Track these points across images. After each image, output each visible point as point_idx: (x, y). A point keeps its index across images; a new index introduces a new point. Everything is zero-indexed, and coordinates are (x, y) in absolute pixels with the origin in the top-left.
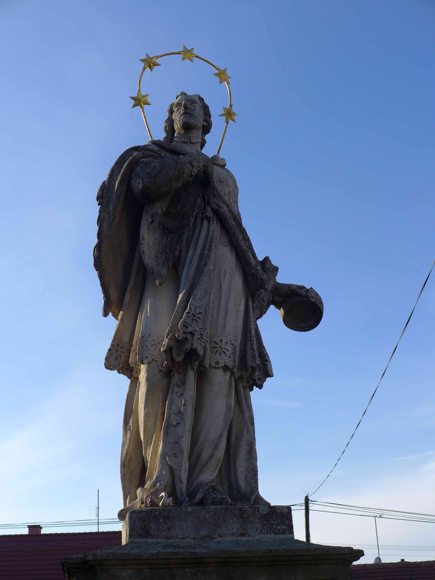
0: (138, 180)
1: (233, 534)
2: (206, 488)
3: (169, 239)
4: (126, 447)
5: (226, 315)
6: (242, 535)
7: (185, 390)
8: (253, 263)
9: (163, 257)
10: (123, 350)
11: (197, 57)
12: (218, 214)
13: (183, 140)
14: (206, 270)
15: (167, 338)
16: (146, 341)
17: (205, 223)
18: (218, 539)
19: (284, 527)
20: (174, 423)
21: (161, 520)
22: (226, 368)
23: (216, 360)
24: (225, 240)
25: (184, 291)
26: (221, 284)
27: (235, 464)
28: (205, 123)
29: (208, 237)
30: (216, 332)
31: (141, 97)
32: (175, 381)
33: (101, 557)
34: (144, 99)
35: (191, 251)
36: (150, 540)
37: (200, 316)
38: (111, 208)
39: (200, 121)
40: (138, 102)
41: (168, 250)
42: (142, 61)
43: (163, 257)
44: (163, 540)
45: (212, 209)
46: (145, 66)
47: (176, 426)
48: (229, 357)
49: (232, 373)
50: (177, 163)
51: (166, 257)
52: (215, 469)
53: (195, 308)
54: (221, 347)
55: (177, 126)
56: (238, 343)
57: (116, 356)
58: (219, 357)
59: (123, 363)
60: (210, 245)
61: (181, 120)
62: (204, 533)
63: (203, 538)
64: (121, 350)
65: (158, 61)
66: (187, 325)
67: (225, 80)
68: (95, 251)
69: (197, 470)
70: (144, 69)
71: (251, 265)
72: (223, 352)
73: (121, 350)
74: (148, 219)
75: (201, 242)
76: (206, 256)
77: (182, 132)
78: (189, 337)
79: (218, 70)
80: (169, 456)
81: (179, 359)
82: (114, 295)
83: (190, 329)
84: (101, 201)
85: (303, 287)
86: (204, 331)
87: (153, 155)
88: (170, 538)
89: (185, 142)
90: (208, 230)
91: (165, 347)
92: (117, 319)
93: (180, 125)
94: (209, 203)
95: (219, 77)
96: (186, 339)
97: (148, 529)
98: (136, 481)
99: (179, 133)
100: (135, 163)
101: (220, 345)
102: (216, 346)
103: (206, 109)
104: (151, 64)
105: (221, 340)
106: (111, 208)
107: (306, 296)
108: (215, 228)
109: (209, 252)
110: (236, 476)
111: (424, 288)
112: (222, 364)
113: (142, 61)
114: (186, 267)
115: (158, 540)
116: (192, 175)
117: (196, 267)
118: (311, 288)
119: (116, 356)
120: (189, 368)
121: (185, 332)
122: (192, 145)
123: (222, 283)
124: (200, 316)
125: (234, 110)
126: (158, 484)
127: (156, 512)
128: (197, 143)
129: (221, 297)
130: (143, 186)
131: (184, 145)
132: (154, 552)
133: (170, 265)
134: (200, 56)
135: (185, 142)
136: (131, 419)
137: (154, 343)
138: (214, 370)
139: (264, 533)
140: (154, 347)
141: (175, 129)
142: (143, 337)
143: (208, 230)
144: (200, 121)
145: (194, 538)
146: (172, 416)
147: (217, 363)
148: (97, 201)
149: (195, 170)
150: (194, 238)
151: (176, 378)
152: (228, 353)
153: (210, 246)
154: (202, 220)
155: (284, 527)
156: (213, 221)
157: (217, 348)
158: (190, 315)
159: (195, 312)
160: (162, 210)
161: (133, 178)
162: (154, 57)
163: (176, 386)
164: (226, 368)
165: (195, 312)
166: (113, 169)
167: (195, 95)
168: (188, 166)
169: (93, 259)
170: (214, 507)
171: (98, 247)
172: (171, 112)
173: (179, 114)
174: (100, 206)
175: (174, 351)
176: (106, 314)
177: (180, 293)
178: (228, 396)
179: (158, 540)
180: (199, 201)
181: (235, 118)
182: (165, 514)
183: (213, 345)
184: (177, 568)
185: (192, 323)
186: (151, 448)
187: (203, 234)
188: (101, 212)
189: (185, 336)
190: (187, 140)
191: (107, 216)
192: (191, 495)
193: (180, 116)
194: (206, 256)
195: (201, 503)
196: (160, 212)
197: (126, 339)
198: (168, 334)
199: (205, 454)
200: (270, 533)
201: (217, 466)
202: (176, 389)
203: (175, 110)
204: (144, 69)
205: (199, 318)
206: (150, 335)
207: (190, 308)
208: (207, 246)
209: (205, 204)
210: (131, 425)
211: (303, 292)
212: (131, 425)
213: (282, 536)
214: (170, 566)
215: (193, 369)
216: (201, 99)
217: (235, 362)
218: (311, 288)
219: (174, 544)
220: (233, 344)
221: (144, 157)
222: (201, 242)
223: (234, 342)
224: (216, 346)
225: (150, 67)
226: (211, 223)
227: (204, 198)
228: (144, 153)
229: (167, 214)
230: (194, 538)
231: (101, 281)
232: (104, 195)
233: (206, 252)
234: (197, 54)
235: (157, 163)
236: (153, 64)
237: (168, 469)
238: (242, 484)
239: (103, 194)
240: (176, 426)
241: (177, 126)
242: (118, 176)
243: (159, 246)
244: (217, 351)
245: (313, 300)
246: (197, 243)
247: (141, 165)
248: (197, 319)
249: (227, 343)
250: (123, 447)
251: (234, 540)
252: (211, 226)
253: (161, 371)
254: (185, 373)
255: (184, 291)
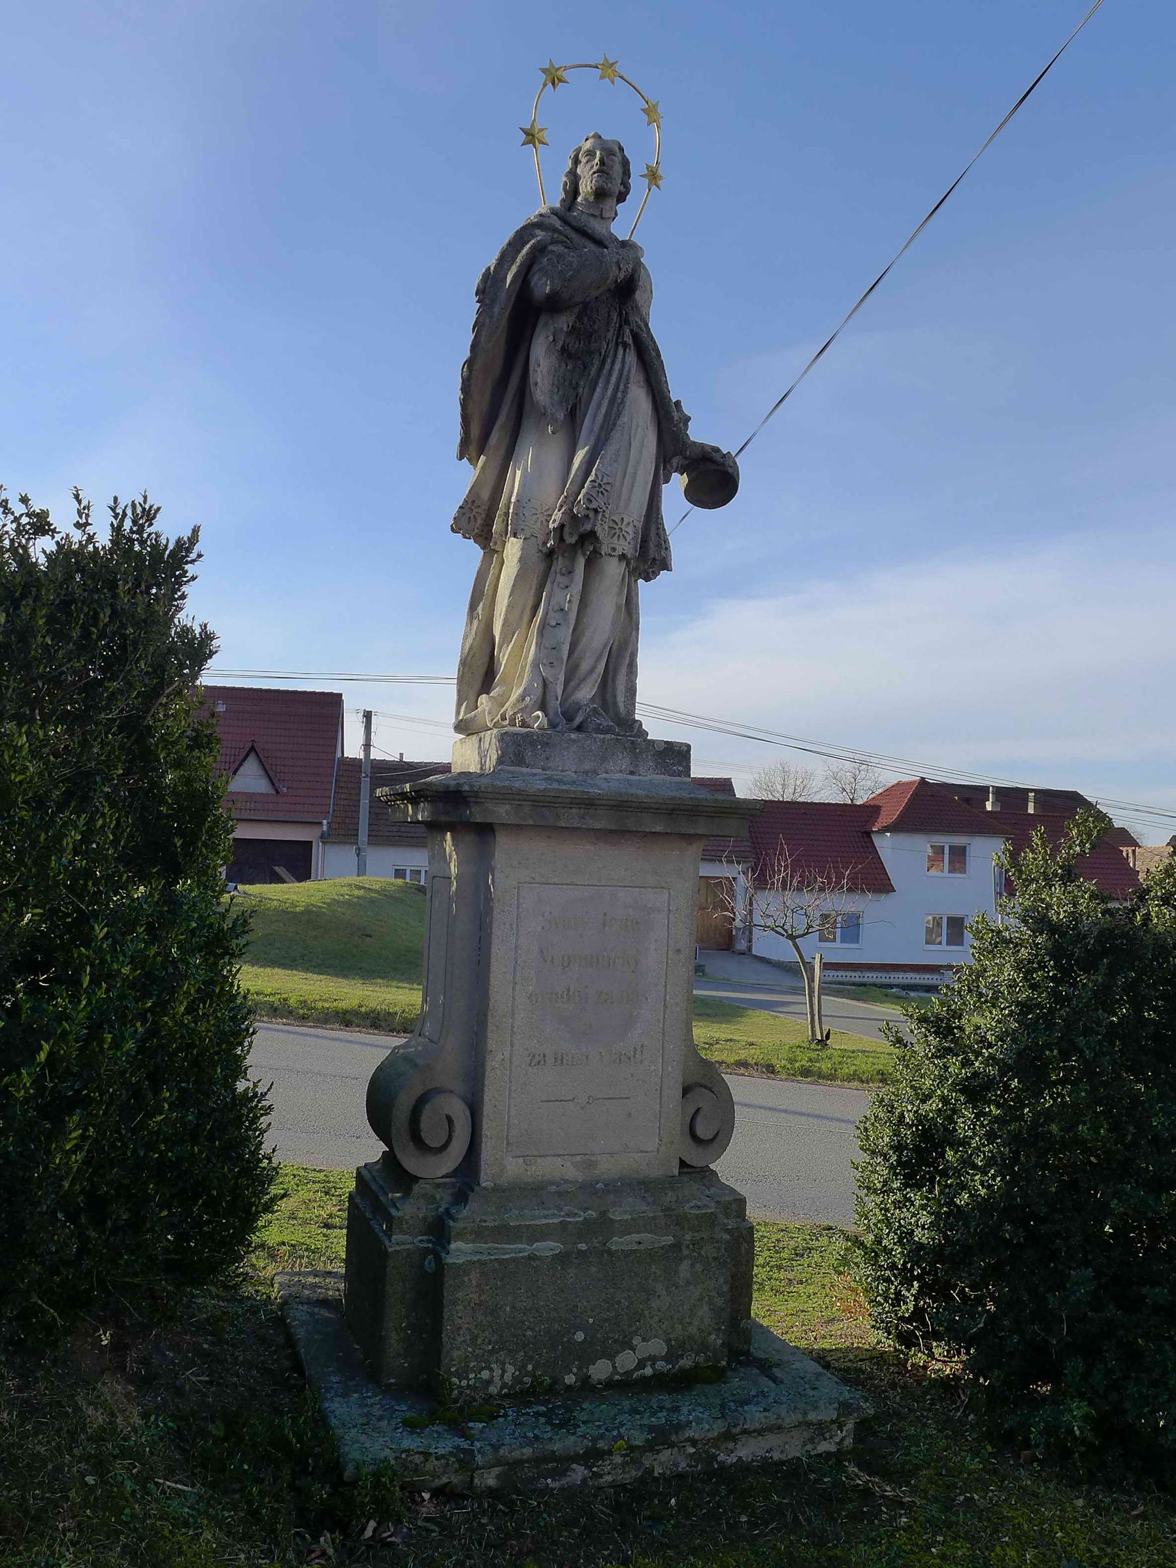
0: (544, 279)
1: (621, 771)
2: (588, 710)
3: (568, 368)
4: (470, 640)
5: (633, 486)
6: (632, 773)
7: (572, 581)
8: (676, 418)
9: (560, 393)
10: (479, 510)
11: (622, 77)
12: (636, 337)
13: (592, 211)
14: (619, 422)
15: (559, 510)
16: (524, 507)
17: (621, 351)
18: (604, 775)
19: (680, 768)
20: (554, 623)
21: (539, 747)
22: (623, 557)
23: (612, 546)
24: (641, 378)
25: (587, 447)
26: (630, 442)
27: (614, 681)
28: (622, 188)
29: (622, 371)
30: (617, 509)
31: (537, 131)
32: (559, 567)
33: (480, 788)
34: (540, 134)
35: (598, 390)
36: (524, 770)
37: (608, 487)
38: (496, 310)
39: (617, 188)
40: (531, 137)
41: (567, 383)
42: (544, 71)
43: (560, 393)
44: (540, 771)
45: (632, 331)
46: (545, 81)
47: (555, 627)
48: (629, 543)
49: (628, 564)
50: (601, 263)
51: (564, 394)
52: (594, 686)
53: (603, 476)
54: (621, 529)
55: (586, 187)
56: (640, 525)
57: (470, 518)
58: (616, 542)
59: (478, 528)
60: (625, 386)
61: (593, 182)
62: (587, 766)
63: (586, 772)
64: (477, 510)
65: (565, 75)
66: (592, 498)
67: (655, 121)
68: (465, 370)
69: (573, 684)
70: (545, 85)
71: (673, 420)
72: (623, 535)
73: (477, 510)
74: (548, 336)
75: (613, 380)
76: (619, 401)
77: (592, 199)
78: (591, 514)
79: (647, 103)
80: (544, 665)
81: (571, 540)
82: (475, 431)
83: (594, 505)
84: (482, 297)
85: (718, 450)
86: (607, 507)
87: (565, 242)
88: (549, 768)
89: (593, 215)
90: (623, 362)
91: (557, 523)
92: (475, 466)
93: (591, 188)
94: (627, 322)
95: (648, 115)
96: (587, 516)
97: (523, 757)
98: (477, 685)
99: (586, 199)
100: (539, 251)
101: (620, 526)
102: (615, 526)
103: (625, 163)
104: (556, 79)
105: (622, 518)
106: (496, 310)
107: (723, 465)
108: (632, 358)
109: (624, 397)
110: (615, 696)
111: (779, 409)
112: (619, 552)
113: (544, 71)
114: (590, 412)
115: (535, 771)
116: (616, 281)
117: (605, 416)
118: (729, 452)
119: (470, 518)
120: (580, 552)
121: (588, 508)
122: (602, 221)
123: (632, 440)
124: (608, 487)
125: (660, 172)
126: (528, 699)
127: (533, 736)
128: (609, 218)
129: (628, 460)
130: (551, 290)
131: (591, 219)
132: (542, 787)
133: (570, 407)
134: (625, 77)
135: (593, 215)
136: (481, 604)
137: (535, 512)
138: (608, 558)
139: (657, 774)
140: (535, 517)
141: (581, 191)
142: (518, 501)
143: (623, 362)
144: (617, 188)
145: (576, 772)
146: (551, 614)
147: (614, 549)
148: (476, 296)
149: (622, 275)
150: (605, 372)
151: (560, 563)
152: (629, 538)
153: (626, 387)
154: (617, 344)
155: (680, 768)
156: (630, 350)
157: (615, 529)
158: (596, 484)
159: (602, 481)
160: (568, 326)
161: (535, 273)
162: (561, 67)
163: (558, 575)
164: (623, 557)
165: (602, 481)
166: (504, 251)
167: (614, 141)
168: (614, 268)
169: (460, 381)
170: (602, 736)
171: (470, 363)
172: (576, 161)
173: (590, 170)
174: (479, 304)
175: (566, 530)
176: (461, 458)
177: (578, 448)
178: (619, 594)
179: (535, 771)
180: (615, 316)
181: (660, 182)
182: (545, 739)
183: (612, 524)
184: (563, 807)
185: (598, 496)
186: (510, 648)
187: (617, 366)
188: (480, 313)
189: (586, 512)
190: (597, 213)
191: (488, 321)
192: (568, 716)
193: (591, 173)
194: (619, 401)
195: (579, 729)
196: (565, 329)
197: (485, 495)
198: (561, 506)
199: (585, 666)
200: (664, 774)
201: (596, 682)
202: (559, 578)
203: (584, 160)
204: (545, 85)
205: (607, 491)
206: (529, 500)
207: (596, 475)
208: (622, 387)
209: (621, 322)
210: (480, 612)
211: (717, 457)
212: (480, 612)
213: (677, 779)
214: (554, 805)
215: (584, 554)
216: (621, 149)
217: (636, 551)
218: (729, 452)
219: (555, 777)
220: (635, 526)
221: (552, 243)
222: (613, 380)
223: (636, 523)
224: (615, 526)
225: (553, 84)
226: (628, 350)
227: (620, 314)
228: (553, 238)
229: (573, 331)
230: (576, 772)
231: (462, 410)
232: (487, 290)
233: (619, 395)
234: (622, 74)
235: (573, 257)
236: (558, 79)
237: (541, 682)
238: (621, 705)
239: (485, 287)
240: (555, 627)
241: (586, 187)
242: (512, 264)
243: (554, 376)
244: (616, 533)
245: (730, 470)
246: (608, 381)
247: (549, 257)
248: (604, 491)
249: (629, 523)
250: (465, 638)
251: (622, 778)
252: (627, 355)
253: (541, 551)
254: (573, 559)
255: (587, 447)
